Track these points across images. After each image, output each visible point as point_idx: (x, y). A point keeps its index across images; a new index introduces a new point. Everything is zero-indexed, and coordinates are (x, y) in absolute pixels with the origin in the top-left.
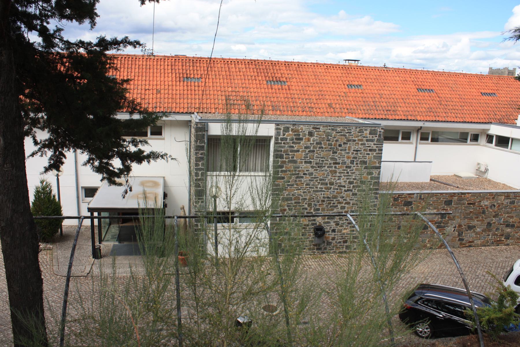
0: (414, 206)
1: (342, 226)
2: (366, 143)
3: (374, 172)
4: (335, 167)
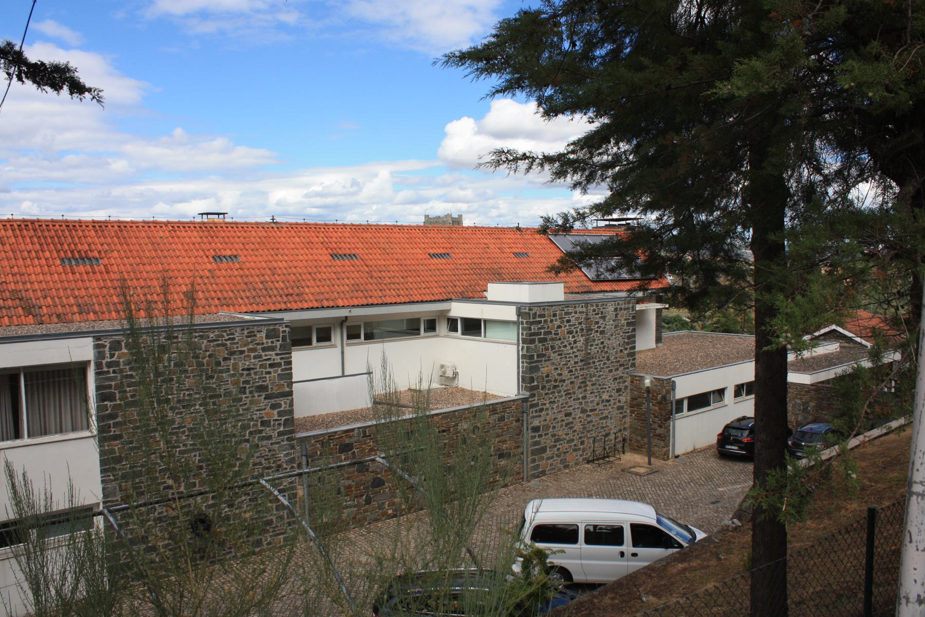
0: (356, 451)
1: (240, 507)
2: (263, 354)
3: (282, 403)
4: (214, 404)
